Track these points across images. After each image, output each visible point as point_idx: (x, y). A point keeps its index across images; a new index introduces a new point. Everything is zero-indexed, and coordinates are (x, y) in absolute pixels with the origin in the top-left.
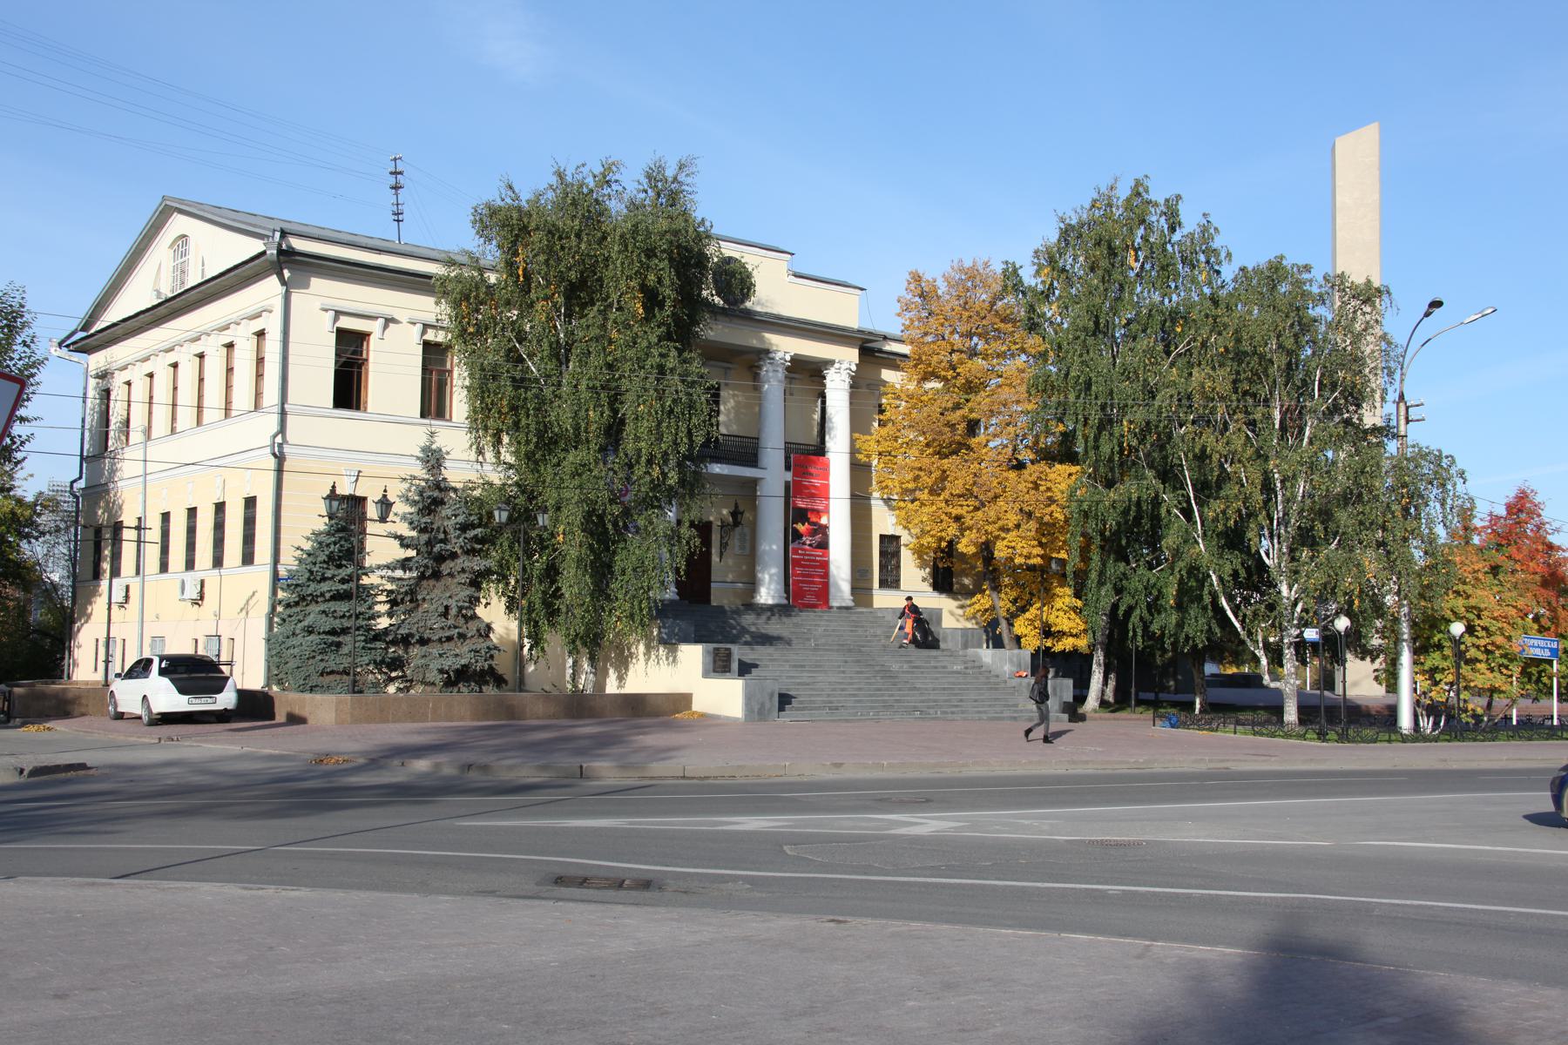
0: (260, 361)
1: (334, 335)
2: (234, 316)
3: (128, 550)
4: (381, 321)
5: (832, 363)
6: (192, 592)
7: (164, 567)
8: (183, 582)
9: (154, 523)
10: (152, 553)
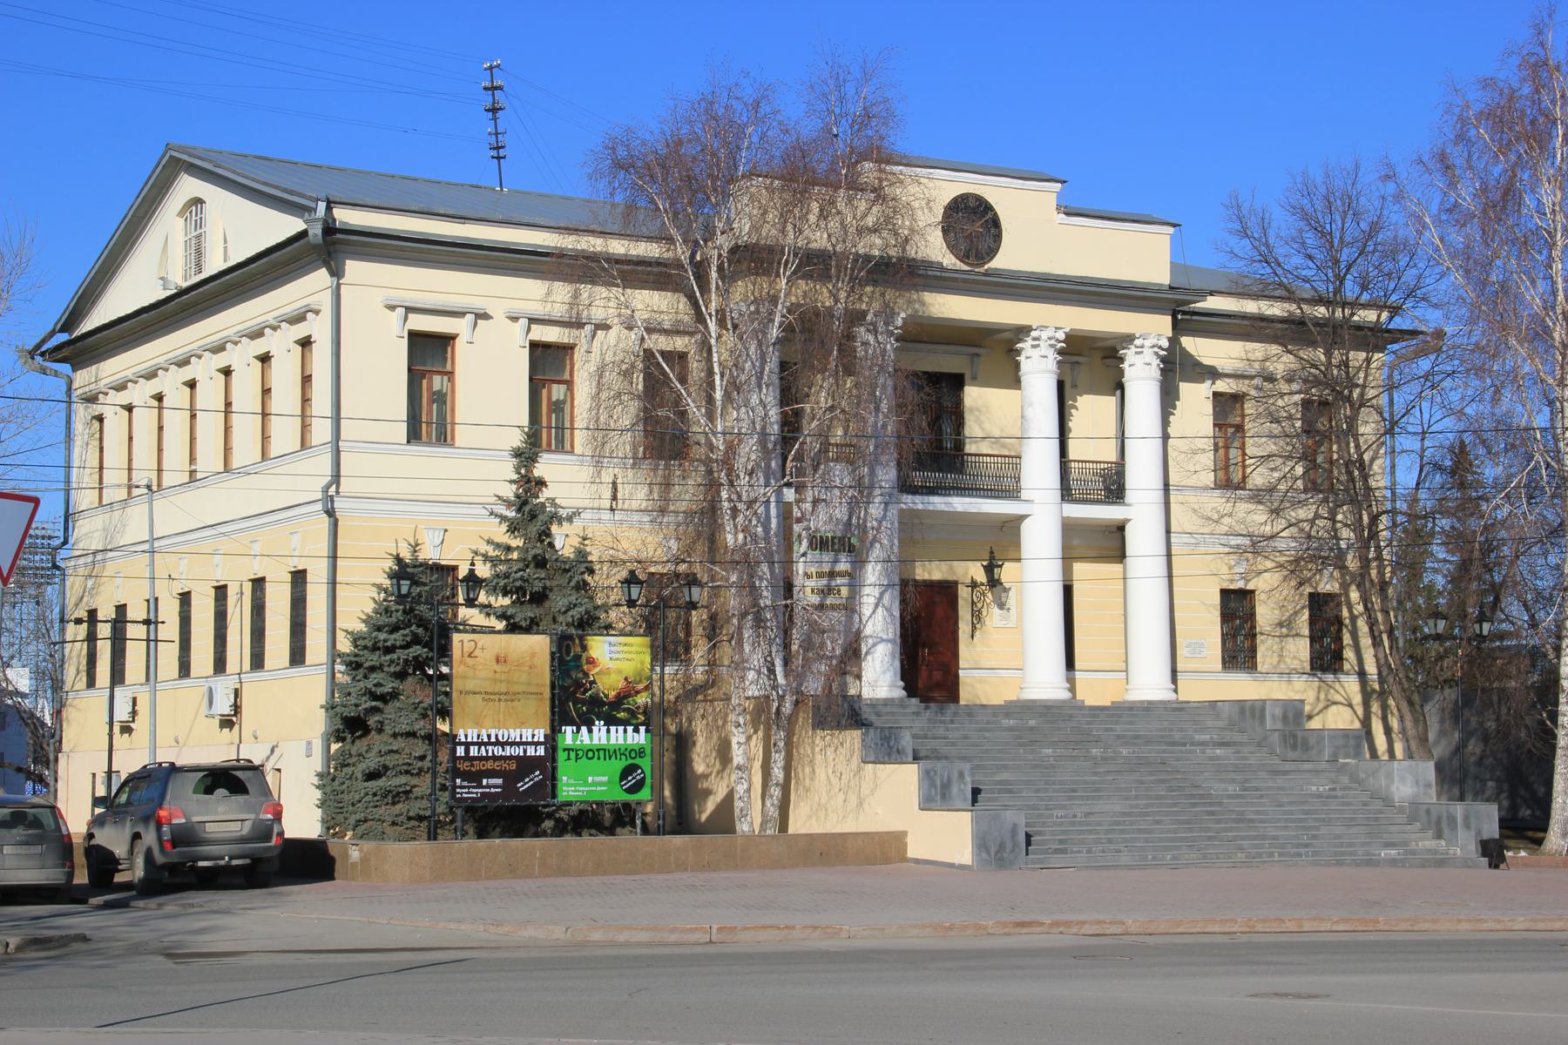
0: (306, 379)
1: (406, 340)
2: (195, 346)
3: (135, 654)
4: (470, 317)
5: (1129, 339)
6: (223, 706)
7: (185, 669)
8: (210, 690)
9: (169, 612)
10: (168, 655)
